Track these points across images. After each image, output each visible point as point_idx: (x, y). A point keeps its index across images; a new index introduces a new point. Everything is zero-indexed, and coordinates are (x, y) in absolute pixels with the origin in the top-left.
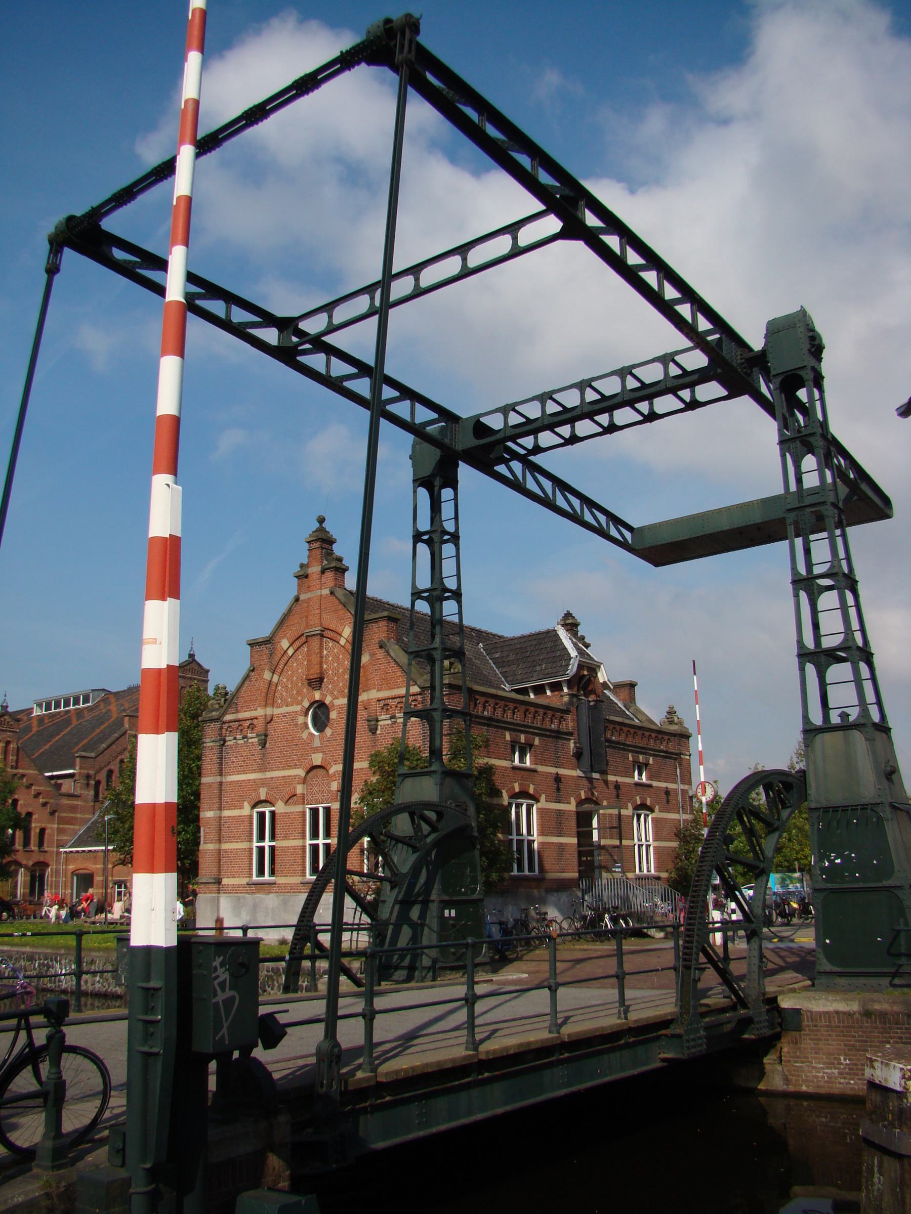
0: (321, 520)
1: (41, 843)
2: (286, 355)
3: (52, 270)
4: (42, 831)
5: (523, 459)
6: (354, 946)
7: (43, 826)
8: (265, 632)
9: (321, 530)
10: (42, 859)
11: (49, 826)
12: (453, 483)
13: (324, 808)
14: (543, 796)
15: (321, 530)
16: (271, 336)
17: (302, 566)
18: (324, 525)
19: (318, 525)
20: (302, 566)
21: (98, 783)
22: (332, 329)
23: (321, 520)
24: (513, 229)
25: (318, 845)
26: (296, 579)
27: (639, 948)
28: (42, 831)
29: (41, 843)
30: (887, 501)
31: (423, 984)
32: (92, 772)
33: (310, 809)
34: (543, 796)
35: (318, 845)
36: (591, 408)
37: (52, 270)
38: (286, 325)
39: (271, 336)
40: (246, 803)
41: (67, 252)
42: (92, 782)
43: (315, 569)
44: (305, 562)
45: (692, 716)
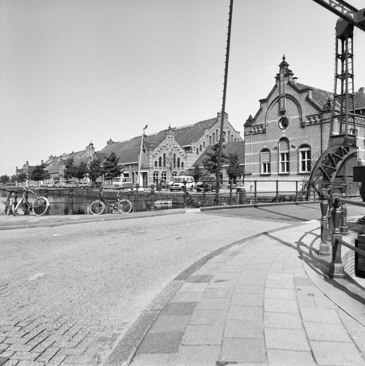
0: (284, 58)
1: (182, 167)
4: (183, 163)
6: (48, 180)
7: (156, 160)
8: (265, 97)
9: (284, 62)
10: (183, 171)
11: (185, 161)
12: (351, 36)
15: (284, 62)
17: (277, 74)
18: (285, 60)
19: (283, 60)
20: (277, 74)
21: (198, 149)
23: (284, 58)
25: (305, 161)
26: (276, 79)
28: (183, 163)
29: (182, 167)
31: (284, 203)
35: (305, 161)
42: (196, 149)
43: (282, 75)
44: (279, 73)
45: (334, 29)
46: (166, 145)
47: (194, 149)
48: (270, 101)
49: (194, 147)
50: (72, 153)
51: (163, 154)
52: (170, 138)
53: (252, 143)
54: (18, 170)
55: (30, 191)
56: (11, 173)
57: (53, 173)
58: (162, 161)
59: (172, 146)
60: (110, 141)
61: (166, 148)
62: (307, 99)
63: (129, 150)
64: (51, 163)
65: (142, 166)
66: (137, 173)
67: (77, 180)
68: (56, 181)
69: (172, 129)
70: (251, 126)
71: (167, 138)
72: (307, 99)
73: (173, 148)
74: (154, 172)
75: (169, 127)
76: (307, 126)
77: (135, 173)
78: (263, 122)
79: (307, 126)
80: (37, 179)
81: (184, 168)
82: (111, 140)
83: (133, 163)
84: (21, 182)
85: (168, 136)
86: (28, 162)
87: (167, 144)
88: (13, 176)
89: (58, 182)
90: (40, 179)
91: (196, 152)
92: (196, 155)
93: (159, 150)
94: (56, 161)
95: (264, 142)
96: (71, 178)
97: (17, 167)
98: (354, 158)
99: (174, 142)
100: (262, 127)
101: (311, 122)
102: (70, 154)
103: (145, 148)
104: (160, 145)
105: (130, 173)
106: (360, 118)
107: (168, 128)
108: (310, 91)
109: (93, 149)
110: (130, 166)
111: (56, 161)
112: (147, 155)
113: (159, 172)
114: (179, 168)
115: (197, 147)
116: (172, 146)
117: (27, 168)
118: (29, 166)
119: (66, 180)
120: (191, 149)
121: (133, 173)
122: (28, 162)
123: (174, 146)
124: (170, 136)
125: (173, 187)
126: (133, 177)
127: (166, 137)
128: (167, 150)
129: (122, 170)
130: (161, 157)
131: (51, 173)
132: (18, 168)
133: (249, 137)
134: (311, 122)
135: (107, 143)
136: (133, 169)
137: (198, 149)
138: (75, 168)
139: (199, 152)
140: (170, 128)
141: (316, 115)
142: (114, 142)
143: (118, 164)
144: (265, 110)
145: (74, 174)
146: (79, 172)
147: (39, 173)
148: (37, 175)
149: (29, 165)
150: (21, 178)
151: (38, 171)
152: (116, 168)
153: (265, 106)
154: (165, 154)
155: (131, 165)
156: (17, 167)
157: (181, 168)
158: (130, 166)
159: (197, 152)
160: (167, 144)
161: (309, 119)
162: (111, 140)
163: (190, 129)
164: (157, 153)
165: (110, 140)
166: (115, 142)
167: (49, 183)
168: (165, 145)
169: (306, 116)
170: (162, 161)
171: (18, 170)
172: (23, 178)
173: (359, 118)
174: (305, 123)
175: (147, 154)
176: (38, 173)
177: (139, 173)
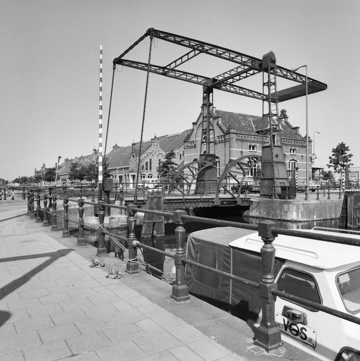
2: (165, 74)
3: (114, 69)
5: (230, 84)
8: (195, 121)
12: (212, 92)
13: (292, 162)
14: (298, 160)
16: (206, 48)
21: (181, 154)
22: (176, 66)
24: (188, 54)
27: (214, 192)
30: (326, 85)
32: (179, 152)
33: (292, 162)
34: (298, 160)
36: (246, 70)
37: (114, 69)
38: (164, 68)
39: (206, 48)
40: (288, 160)
41: (117, 65)
42: (179, 154)
46: (152, 152)
47: (178, 155)
48: (198, 124)
49: (178, 153)
50: (81, 157)
51: (149, 159)
52: (156, 146)
53: (188, 155)
54: (36, 172)
55: (6, 188)
56: (30, 174)
57: (63, 175)
58: (149, 165)
59: (157, 152)
60: (115, 146)
61: (152, 154)
62: (218, 124)
63: (125, 155)
64: (63, 166)
65: (132, 170)
66: (128, 175)
67: (78, 181)
68: (64, 182)
69: (157, 138)
70: (188, 142)
71: (153, 146)
72: (218, 124)
73: (158, 154)
74: (149, 175)
75: (155, 137)
76: (218, 143)
77: (127, 176)
78: (194, 140)
79: (218, 143)
80: (49, 180)
81: (152, 171)
82: (116, 145)
83: (112, 168)
84: (37, 183)
85: (153, 144)
86: (44, 164)
87: (153, 151)
88: (31, 177)
89: (65, 183)
90: (51, 180)
91: (179, 157)
92: (179, 160)
93: (146, 156)
94: (68, 164)
95: (195, 154)
96: (75, 180)
97: (35, 169)
98: (213, 169)
99: (159, 149)
100: (194, 143)
101: (220, 141)
102: (79, 158)
103: (134, 154)
104: (147, 151)
105: (123, 175)
106: (259, 137)
107: (154, 137)
108: (219, 118)
109: (96, 154)
110: (123, 170)
111: (68, 164)
112: (135, 160)
113: (146, 175)
114: (151, 171)
115: (180, 153)
116: (157, 152)
117: (44, 170)
118: (46, 168)
119: (71, 181)
120: (175, 155)
121: (125, 175)
122: (44, 164)
123: (159, 152)
124: (156, 144)
125: (140, 187)
126: (126, 178)
127: (152, 145)
128: (153, 156)
129: (111, 173)
130: (147, 162)
131: (60, 175)
132: (37, 170)
133: (186, 149)
134: (220, 141)
135: (113, 147)
136: (125, 172)
137: (181, 154)
138: (77, 171)
139: (182, 157)
140: (155, 137)
141: (222, 136)
142: (119, 147)
143: (108, 169)
144: (195, 130)
145: (75, 176)
146: (80, 174)
147: (51, 175)
148: (50, 177)
149: (46, 167)
150: (38, 179)
151: (50, 173)
152: (106, 172)
153: (196, 127)
154: (151, 159)
155: (124, 168)
156: (35, 169)
157: (149, 171)
158: (123, 170)
159: (180, 158)
160: (153, 151)
161: (219, 138)
162: (116, 145)
163: (178, 137)
164: (144, 158)
165: (115, 145)
166: (120, 146)
167: (58, 183)
168: (151, 152)
169: (217, 136)
170: (149, 165)
171: (36, 172)
172: (38, 179)
173: (258, 137)
174: (216, 141)
175: (136, 159)
176: (50, 175)
177: (130, 176)
